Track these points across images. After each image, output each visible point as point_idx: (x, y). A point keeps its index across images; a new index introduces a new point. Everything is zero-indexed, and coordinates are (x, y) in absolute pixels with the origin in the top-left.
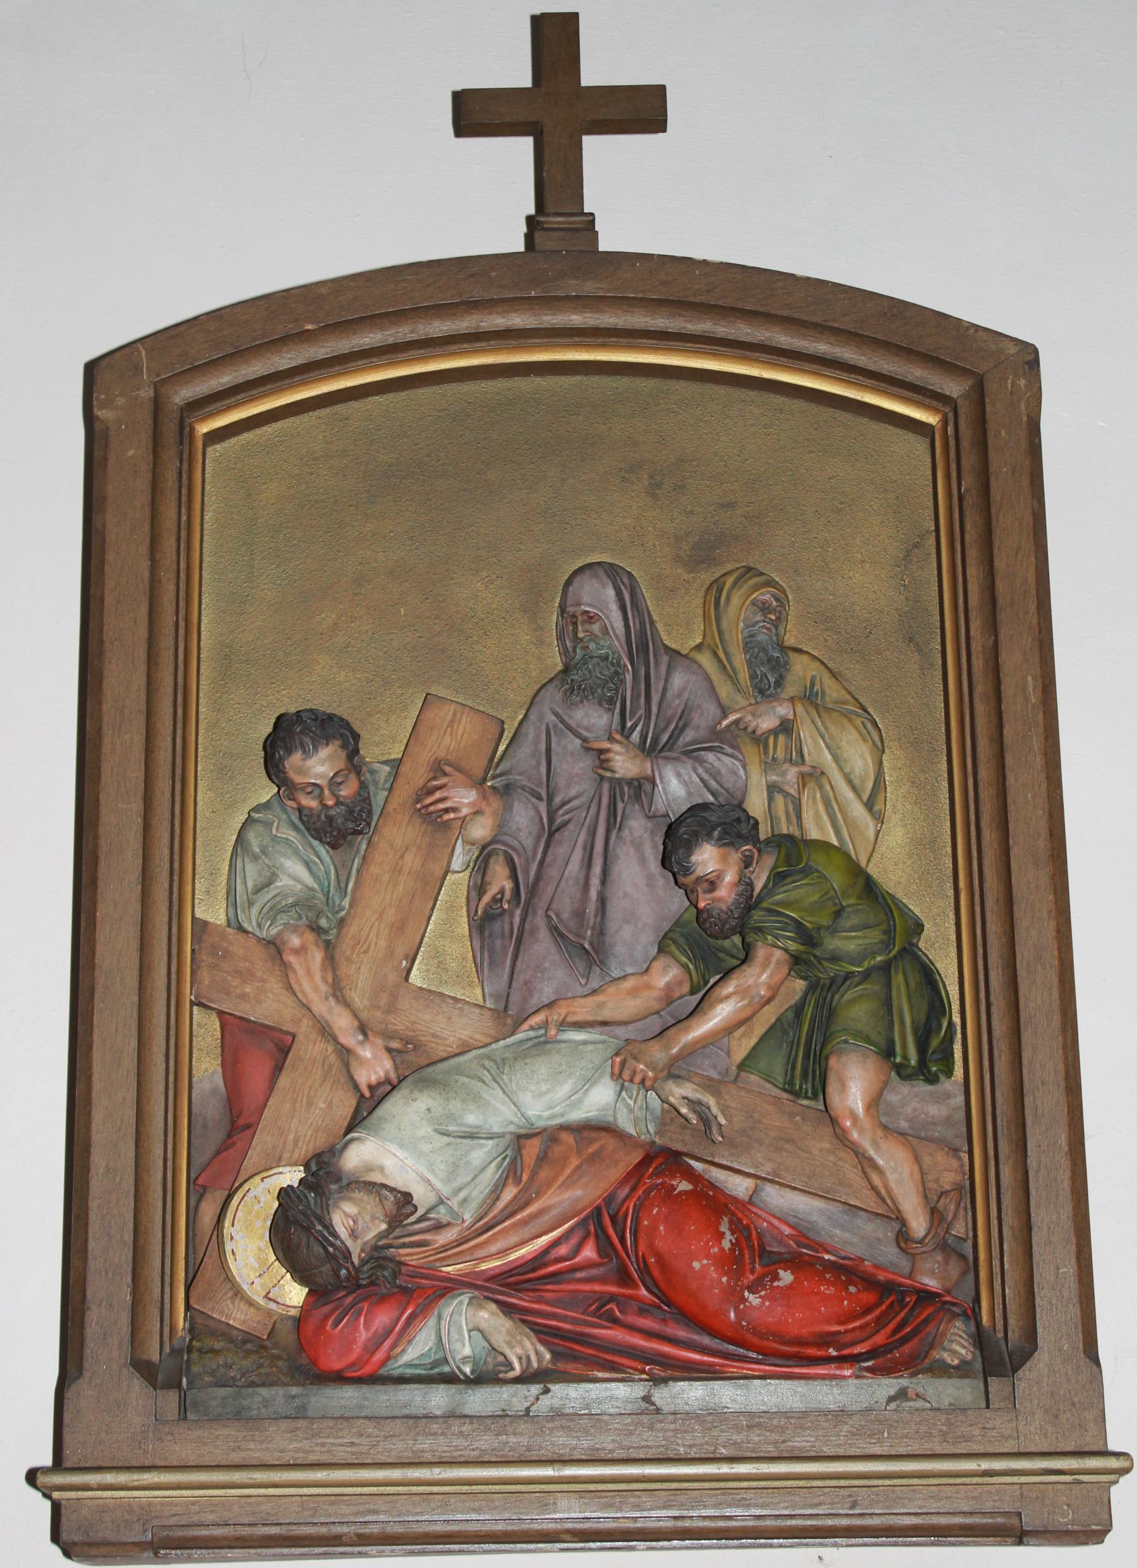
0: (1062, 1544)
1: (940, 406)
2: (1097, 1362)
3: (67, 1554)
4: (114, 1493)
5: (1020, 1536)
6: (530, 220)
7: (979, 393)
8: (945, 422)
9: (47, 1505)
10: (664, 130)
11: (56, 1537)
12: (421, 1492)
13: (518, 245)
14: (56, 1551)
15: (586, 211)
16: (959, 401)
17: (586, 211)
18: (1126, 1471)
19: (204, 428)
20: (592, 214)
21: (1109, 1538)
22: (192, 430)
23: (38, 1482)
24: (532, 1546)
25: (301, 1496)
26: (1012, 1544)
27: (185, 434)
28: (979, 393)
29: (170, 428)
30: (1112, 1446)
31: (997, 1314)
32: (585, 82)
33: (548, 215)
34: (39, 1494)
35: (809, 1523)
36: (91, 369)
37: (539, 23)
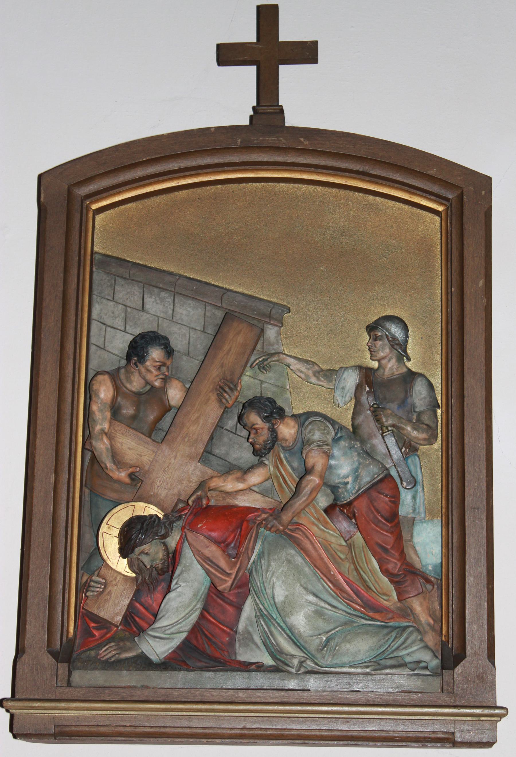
0: (255, 744)
1: (444, 202)
2: (494, 664)
3: (15, 737)
4: (43, 711)
5: (455, 744)
6: (254, 108)
7: (461, 197)
8: (447, 210)
9: (8, 715)
10: (317, 63)
11: (11, 730)
12: (148, 714)
13: (247, 122)
14: (11, 735)
15: (280, 104)
16: (453, 201)
17: (280, 104)
18: (504, 715)
19: (95, 207)
20: (281, 106)
21: (494, 746)
22: (88, 208)
23: (4, 705)
24: (404, 744)
25: (133, 715)
26: (450, 747)
27: (84, 210)
28: (461, 197)
29: (77, 207)
30: (499, 704)
31: (68, 591)
32: (281, 39)
33: (262, 106)
34: (4, 710)
35: (251, 732)
36: (40, 177)
37: (261, 10)
